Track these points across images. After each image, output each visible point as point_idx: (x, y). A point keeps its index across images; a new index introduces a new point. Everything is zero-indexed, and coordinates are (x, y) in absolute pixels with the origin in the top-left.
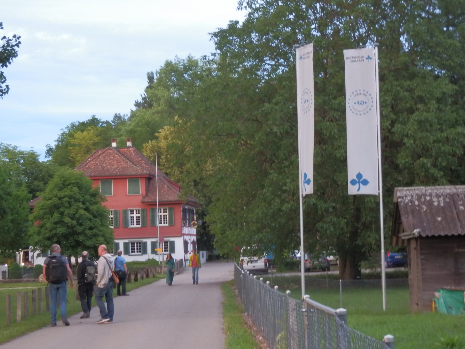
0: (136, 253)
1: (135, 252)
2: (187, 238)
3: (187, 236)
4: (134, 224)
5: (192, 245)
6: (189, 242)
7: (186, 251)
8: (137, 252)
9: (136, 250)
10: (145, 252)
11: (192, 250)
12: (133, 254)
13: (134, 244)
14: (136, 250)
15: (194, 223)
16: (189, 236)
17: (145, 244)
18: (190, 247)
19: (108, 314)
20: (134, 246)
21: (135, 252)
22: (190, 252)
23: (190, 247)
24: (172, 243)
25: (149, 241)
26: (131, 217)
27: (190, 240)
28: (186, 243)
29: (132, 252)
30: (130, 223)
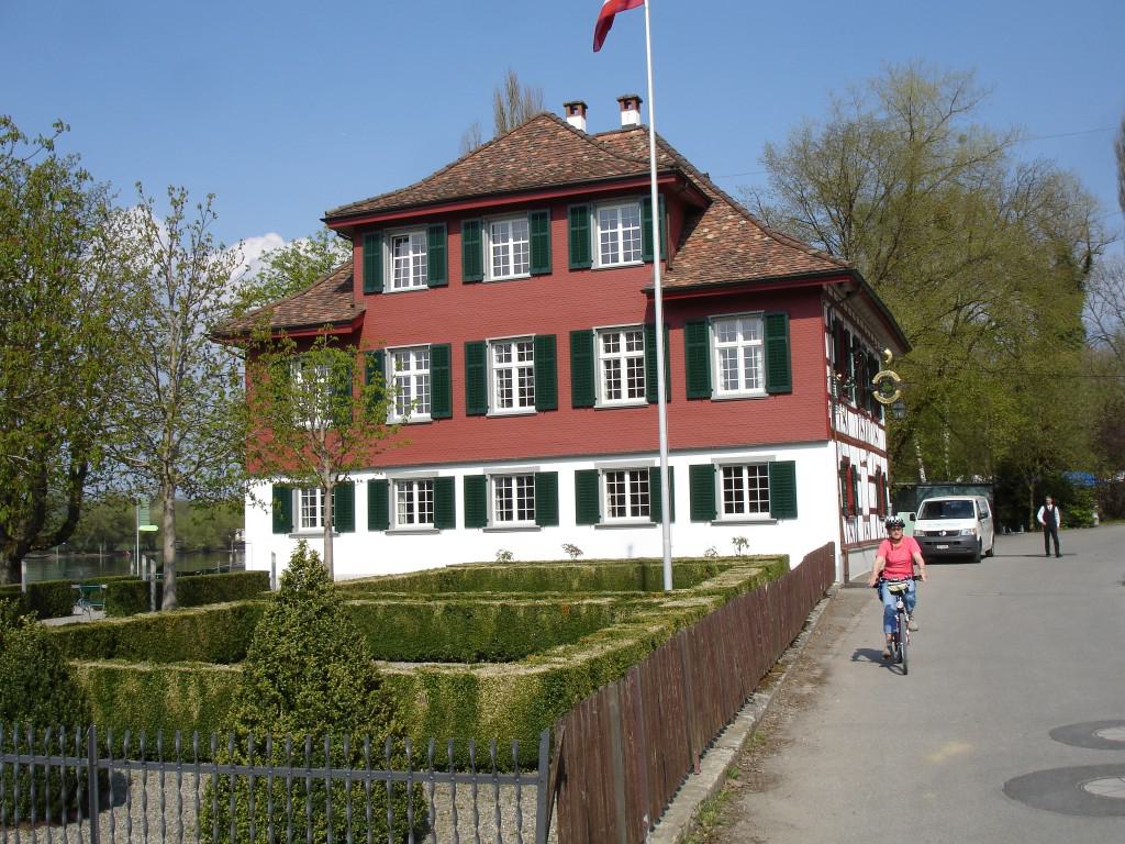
0: (747, 515)
1: (740, 509)
2: (856, 455)
3: (853, 448)
4: (618, 395)
5: (873, 486)
6: (864, 473)
7: (850, 509)
8: (635, 512)
9: (746, 501)
10: (546, 513)
11: (874, 505)
12: (734, 516)
13: (738, 471)
14: (746, 501)
15: (890, 393)
16: (863, 451)
17: (550, 481)
18: (867, 495)
19: (1053, 550)
20: (739, 484)
21: (740, 509)
22: (866, 511)
23: (867, 495)
24: (786, 472)
25: (566, 474)
26: (608, 363)
27: (864, 464)
28: (848, 474)
29: (729, 509)
30: (394, 366)
